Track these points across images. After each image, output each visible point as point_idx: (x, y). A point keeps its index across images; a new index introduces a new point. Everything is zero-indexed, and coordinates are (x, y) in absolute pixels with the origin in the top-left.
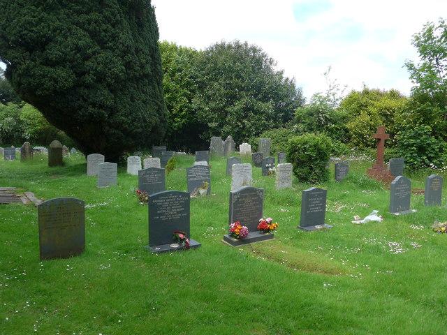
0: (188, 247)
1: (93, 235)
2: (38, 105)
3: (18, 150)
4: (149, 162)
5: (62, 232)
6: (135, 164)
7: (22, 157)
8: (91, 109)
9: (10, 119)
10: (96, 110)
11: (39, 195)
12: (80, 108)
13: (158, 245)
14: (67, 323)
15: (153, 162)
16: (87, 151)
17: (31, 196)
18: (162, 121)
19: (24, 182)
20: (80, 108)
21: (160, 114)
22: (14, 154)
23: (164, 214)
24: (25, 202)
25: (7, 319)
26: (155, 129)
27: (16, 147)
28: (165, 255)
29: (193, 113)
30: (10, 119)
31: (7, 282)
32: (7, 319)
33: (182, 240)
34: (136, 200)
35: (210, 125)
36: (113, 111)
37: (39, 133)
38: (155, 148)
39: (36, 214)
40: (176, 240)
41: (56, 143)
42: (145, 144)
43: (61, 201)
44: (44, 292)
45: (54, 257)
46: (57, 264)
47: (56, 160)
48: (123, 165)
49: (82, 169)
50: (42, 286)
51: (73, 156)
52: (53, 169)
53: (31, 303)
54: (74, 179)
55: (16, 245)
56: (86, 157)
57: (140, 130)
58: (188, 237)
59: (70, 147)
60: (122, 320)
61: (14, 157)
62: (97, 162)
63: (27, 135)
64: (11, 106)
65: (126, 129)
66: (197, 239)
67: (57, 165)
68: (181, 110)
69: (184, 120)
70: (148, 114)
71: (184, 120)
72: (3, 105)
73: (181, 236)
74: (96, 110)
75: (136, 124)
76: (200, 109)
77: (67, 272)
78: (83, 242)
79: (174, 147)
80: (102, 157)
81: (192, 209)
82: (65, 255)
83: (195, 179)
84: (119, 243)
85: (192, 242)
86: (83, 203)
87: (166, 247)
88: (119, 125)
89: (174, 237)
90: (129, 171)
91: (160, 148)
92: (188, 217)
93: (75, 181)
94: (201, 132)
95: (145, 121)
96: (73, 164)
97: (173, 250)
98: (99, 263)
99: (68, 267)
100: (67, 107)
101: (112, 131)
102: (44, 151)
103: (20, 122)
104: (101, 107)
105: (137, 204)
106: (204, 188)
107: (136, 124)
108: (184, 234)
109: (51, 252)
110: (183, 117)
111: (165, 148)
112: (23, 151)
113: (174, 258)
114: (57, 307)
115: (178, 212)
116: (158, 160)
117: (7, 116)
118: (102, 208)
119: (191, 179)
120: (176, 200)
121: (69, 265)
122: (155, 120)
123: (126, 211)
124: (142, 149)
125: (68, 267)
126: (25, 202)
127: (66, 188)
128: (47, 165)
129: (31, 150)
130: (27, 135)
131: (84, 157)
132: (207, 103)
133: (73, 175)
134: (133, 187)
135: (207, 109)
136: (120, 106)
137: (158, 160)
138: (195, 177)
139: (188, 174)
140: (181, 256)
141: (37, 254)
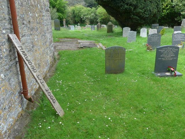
0: (175, 75)
1: (128, 64)
2: (104, 6)
3: (96, 26)
4: (151, 31)
5: (115, 61)
6: (144, 32)
7: (97, 29)
8: (126, 6)
9: (93, 14)
10: (128, 7)
11: (104, 45)
12: (121, 6)
13: (159, 72)
14: (119, 108)
15: (153, 31)
16: (123, 26)
17: (101, 45)
18: (159, 11)
19: (98, 39)
20: (121, 6)
21: (158, 8)
22: (94, 28)
23: (164, 57)
24: (98, 47)
25: (93, 100)
26: (155, 15)
27: (95, 25)
28: (163, 78)
29: (173, 7)
30: (93, 14)
31: (92, 81)
32: (93, 100)
33: (172, 71)
34: (145, 49)
35: (182, 13)
36: (136, 7)
37: (103, 19)
38: (153, 25)
39: (104, 53)
40: (168, 71)
41: (110, 23)
42: (149, 23)
43: (115, 47)
44: (107, 89)
45: (111, 73)
46: (113, 76)
47: (110, 30)
48: (139, 33)
49: (121, 34)
50: (108, 87)
51: (117, 29)
52: (109, 34)
53: (102, 94)
54: (117, 38)
55: (95, 65)
56: (123, 29)
57: (147, 16)
58: (175, 69)
59: (116, 24)
60: (146, 112)
61: (94, 29)
62: (127, 31)
63: (99, 20)
64: (94, 8)
65: (141, 15)
66: (179, 71)
67: (110, 32)
68: (167, 6)
69: (168, 11)
70: (152, 8)
71: (168, 11)
72: (91, 9)
73: (172, 69)
74: (128, 7)
75: (146, 13)
76: (177, 5)
77: (117, 81)
78: (123, 67)
79: (161, 24)
80: (129, 29)
81: (179, 56)
82: (116, 72)
83: (177, 40)
84: (139, 69)
85: (177, 73)
86: (125, 49)
87: (163, 74)
88: (138, 14)
89: (168, 70)
90: (141, 35)
91: (155, 25)
92: (177, 60)
93: (118, 39)
94: (176, 17)
95: (150, 11)
96: (116, 32)
97: (167, 76)
98: (130, 79)
99: (117, 79)
100: (116, 6)
101: (135, 17)
102: (105, 27)
103: (96, 15)
104: (130, 5)
105: (146, 51)
106: (181, 45)
107: (146, 13)
108: (174, 69)
109: (109, 71)
110: (168, 9)
111: (158, 25)
112: (98, 27)
113: (167, 79)
114: (114, 98)
115: (172, 57)
116: (156, 30)
117: (92, 13)
118: (130, 52)
119: (175, 40)
120: (171, 51)
121: (119, 78)
122: (155, 11)
123: (141, 54)
124: (146, 26)
125: (117, 79)
126: (98, 47)
127: (114, 42)
128: (106, 32)
129: (101, 26)
130: (99, 20)
131: (122, 29)
132: (181, 2)
133: (117, 37)
134: (144, 43)
135: (181, 5)
136: (139, 4)
137: (156, 30)
138: (177, 39)
139: (173, 37)
140: (171, 79)
141: (104, 71)
